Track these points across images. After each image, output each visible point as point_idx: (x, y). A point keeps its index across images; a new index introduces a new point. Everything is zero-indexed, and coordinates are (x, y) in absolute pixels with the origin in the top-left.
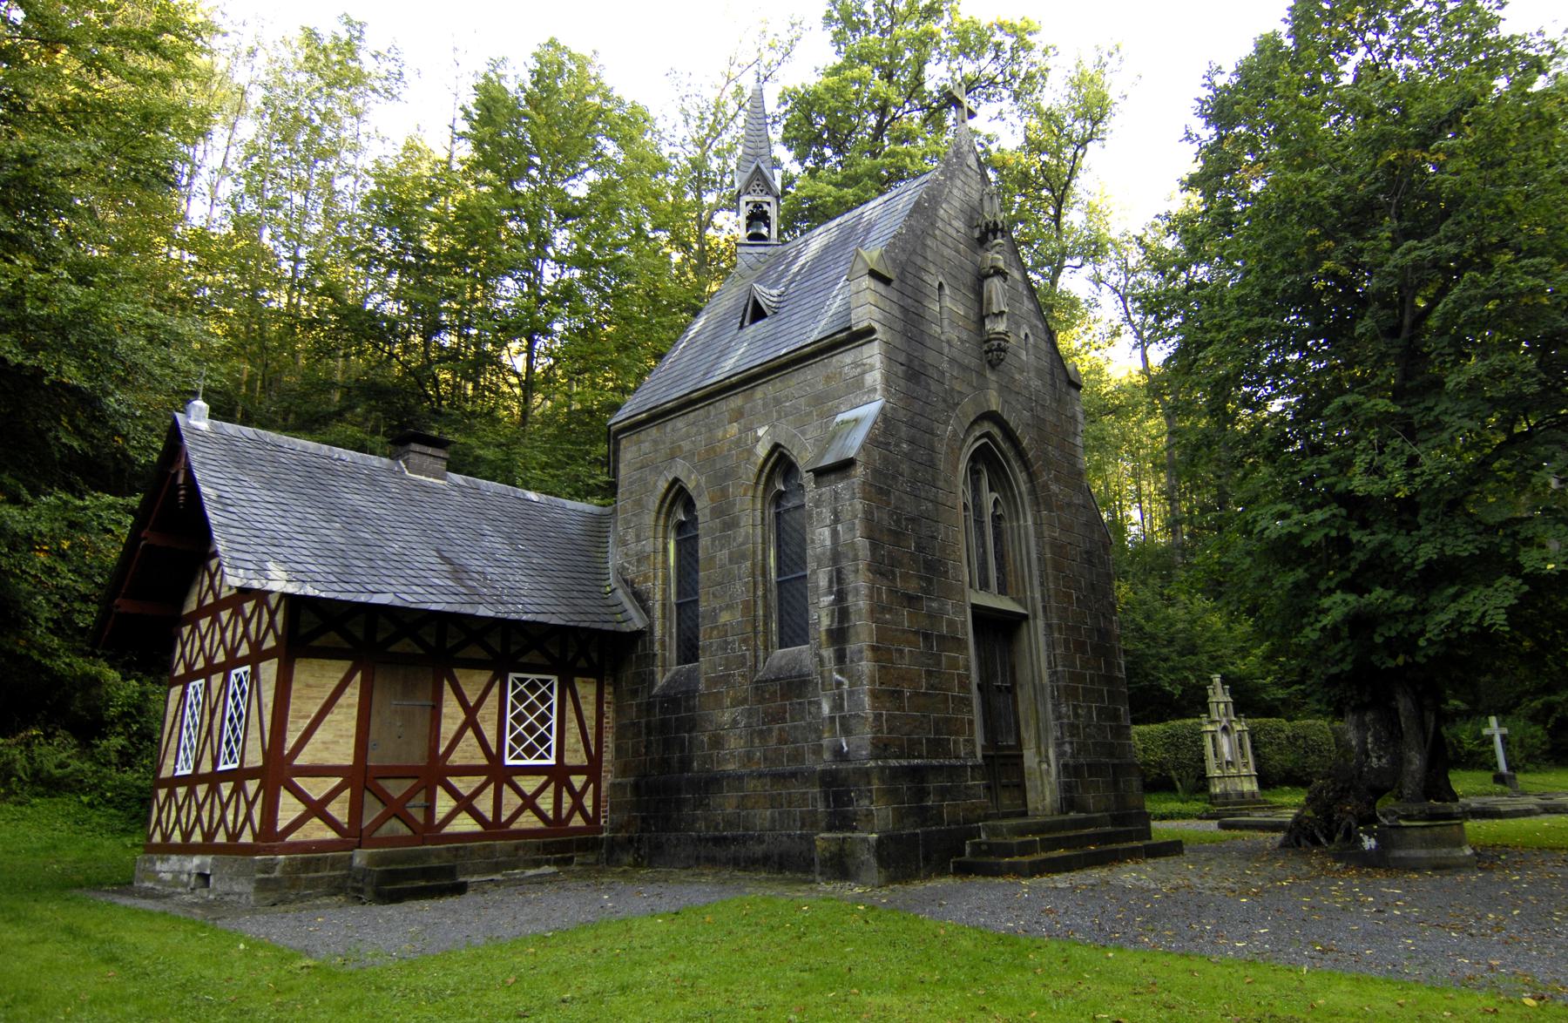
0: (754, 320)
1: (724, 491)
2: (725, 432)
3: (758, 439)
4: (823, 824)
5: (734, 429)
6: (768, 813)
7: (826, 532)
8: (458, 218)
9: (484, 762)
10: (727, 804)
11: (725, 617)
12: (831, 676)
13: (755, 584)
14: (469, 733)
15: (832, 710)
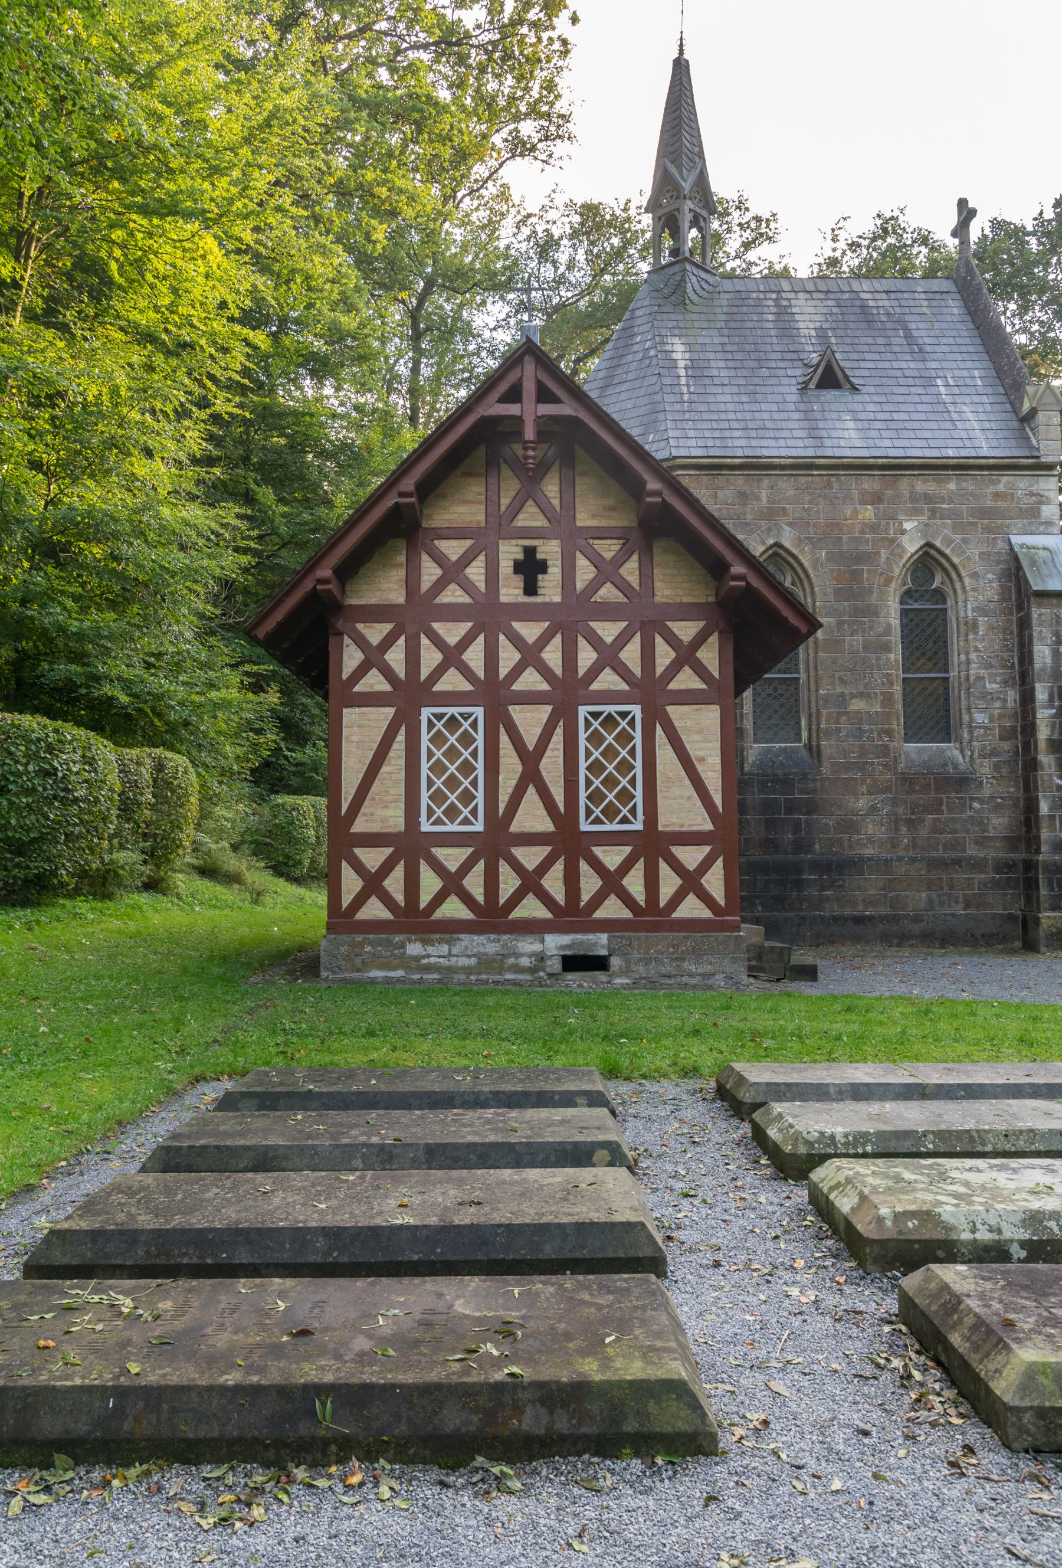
0: (820, 386)
1: (856, 576)
2: (856, 513)
3: (903, 532)
4: (1046, 905)
5: (868, 513)
6: (924, 895)
7: (1047, 651)
8: (975, 255)
9: (709, 826)
10: (871, 884)
11: (857, 705)
12: (1051, 780)
13: (816, 668)
14: (531, 791)
15: (1050, 809)
